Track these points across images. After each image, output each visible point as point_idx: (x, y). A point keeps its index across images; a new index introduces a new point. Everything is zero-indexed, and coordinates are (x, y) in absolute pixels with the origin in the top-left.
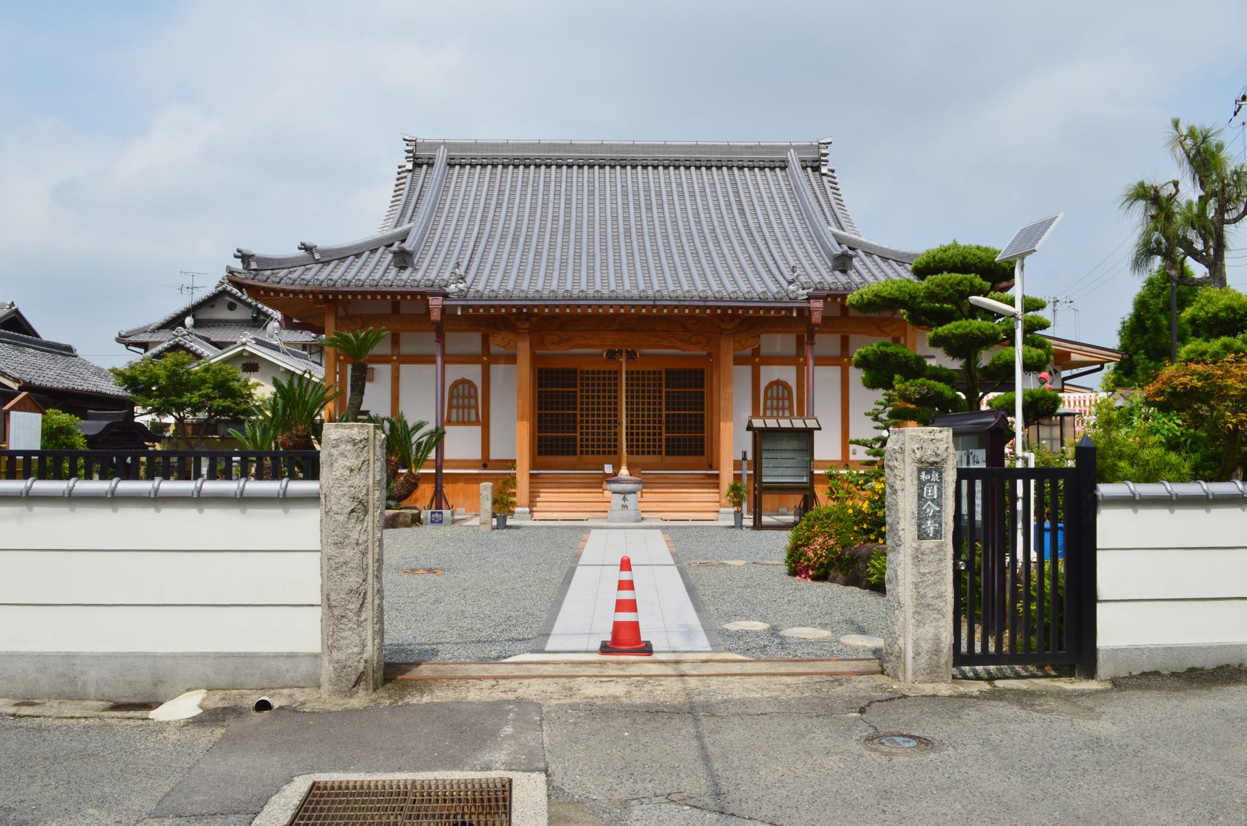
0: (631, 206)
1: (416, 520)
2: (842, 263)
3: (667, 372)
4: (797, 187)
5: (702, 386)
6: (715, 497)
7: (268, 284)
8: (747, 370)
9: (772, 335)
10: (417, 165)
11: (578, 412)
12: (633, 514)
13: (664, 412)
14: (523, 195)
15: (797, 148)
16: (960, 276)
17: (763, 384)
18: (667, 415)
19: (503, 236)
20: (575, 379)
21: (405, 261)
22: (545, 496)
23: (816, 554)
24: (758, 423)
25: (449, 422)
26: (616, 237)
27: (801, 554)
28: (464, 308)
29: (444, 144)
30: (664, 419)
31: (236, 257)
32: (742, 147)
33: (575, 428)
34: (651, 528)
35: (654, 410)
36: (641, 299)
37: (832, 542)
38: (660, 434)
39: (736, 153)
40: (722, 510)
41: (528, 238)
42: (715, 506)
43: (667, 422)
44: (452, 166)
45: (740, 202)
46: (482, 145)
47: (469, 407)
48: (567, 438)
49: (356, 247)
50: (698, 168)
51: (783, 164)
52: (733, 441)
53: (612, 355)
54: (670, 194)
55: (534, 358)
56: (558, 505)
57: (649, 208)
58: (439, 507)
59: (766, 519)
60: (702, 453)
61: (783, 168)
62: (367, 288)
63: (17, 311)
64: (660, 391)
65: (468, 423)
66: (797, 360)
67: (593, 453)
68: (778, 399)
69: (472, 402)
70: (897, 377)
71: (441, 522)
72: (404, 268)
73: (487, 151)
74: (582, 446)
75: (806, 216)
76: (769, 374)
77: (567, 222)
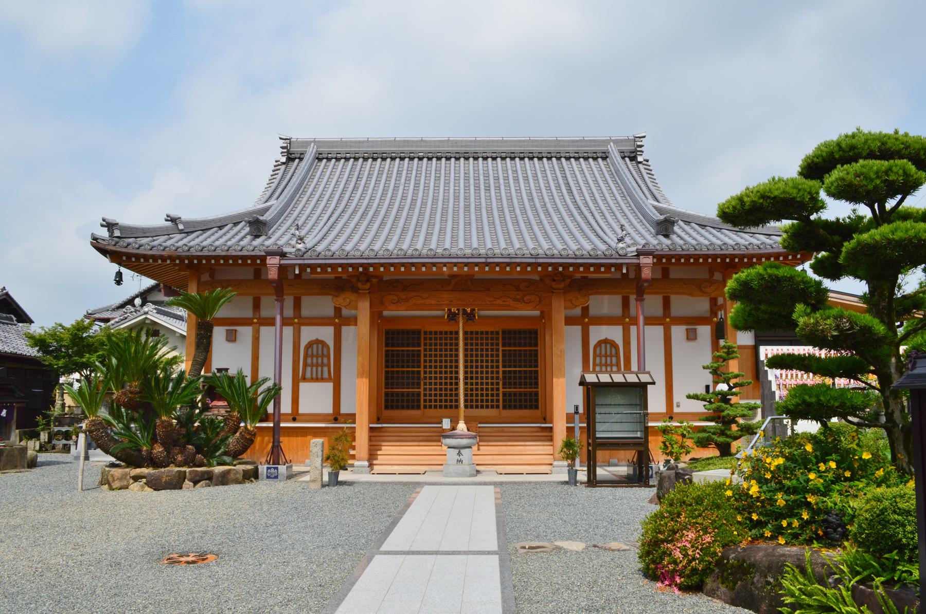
0: (472, 187)
1: (253, 475)
2: (665, 226)
3: (504, 332)
4: (617, 171)
5: (536, 345)
6: (549, 450)
7: (130, 250)
8: (577, 330)
9: (600, 296)
10: (290, 159)
11: (422, 369)
12: (467, 468)
13: (501, 369)
14: (378, 181)
15: (616, 142)
16: (885, 164)
17: (593, 342)
18: (504, 372)
19: (355, 211)
20: (419, 339)
21: (259, 230)
22: (388, 450)
23: (686, 555)
24: (591, 378)
25: (304, 379)
26: (456, 212)
27: (664, 553)
28: (303, 267)
29: (315, 142)
30: (501, 376)
31: (102, 226)
32: (568, 141)
33: (419, 384)
34: (485, 484)
35: (492, 367)
36: (473, 257)
37: (708, 538)
38: (498, 389)
39: (563, 146)
40: (555, 463)
41: (377, 212)
42: (548, 459)
43: (504, 378)
44: (320, 160)
45: (568, 184)
46: (346, 142)
47: (323, 365)
48: (407, 393)
49: (220, 220)
50: (531, 159)
51: (604, 155)
52: (565, 396)
53: (453, 317)
54: (506, 178)
55: (376, 317)
56: (398, 459)
57: (488, 189)
58: (277, 462)
59: (601, 472)
60: (537, 407)
61: (604, 159)
62: (219, 252)
63: (7, 294)
64: (498, 350)
65: (322, 380)
66: (625, 320)
67: (435, 407)
68: (606, 356)
69: (325, 360)
70: (800, 307)
71: (276, 477)
72: (257, 236)
73: (351, 147)
74: (425, 401)
75: (628, 194)
76: (598, 333)
77: (414, 201)
